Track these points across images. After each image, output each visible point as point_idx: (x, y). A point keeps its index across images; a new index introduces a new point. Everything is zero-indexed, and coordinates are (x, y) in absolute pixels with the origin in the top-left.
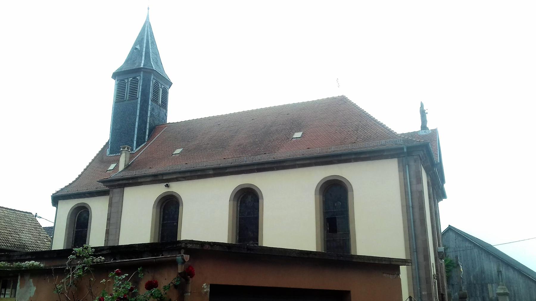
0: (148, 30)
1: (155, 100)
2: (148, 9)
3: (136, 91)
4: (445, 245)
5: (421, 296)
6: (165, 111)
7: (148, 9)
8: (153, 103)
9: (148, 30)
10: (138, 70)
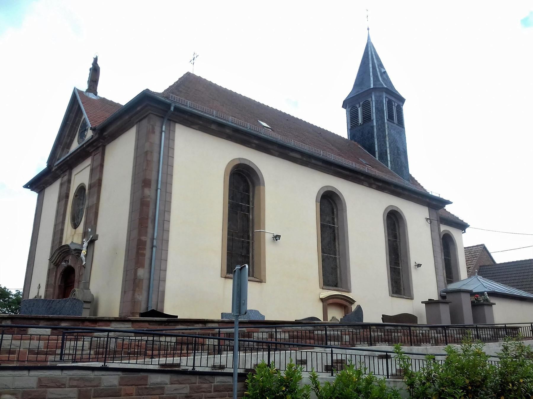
0: (371, 50)
1: (391, 117)
2: (368, 29)
3: (369, 109)
4: (409, 384)
5: (13, 303)
6: (387, 162)
7: (368, 29)
8: (389, 123)
9: (371, 50)
10: (369, 92)
